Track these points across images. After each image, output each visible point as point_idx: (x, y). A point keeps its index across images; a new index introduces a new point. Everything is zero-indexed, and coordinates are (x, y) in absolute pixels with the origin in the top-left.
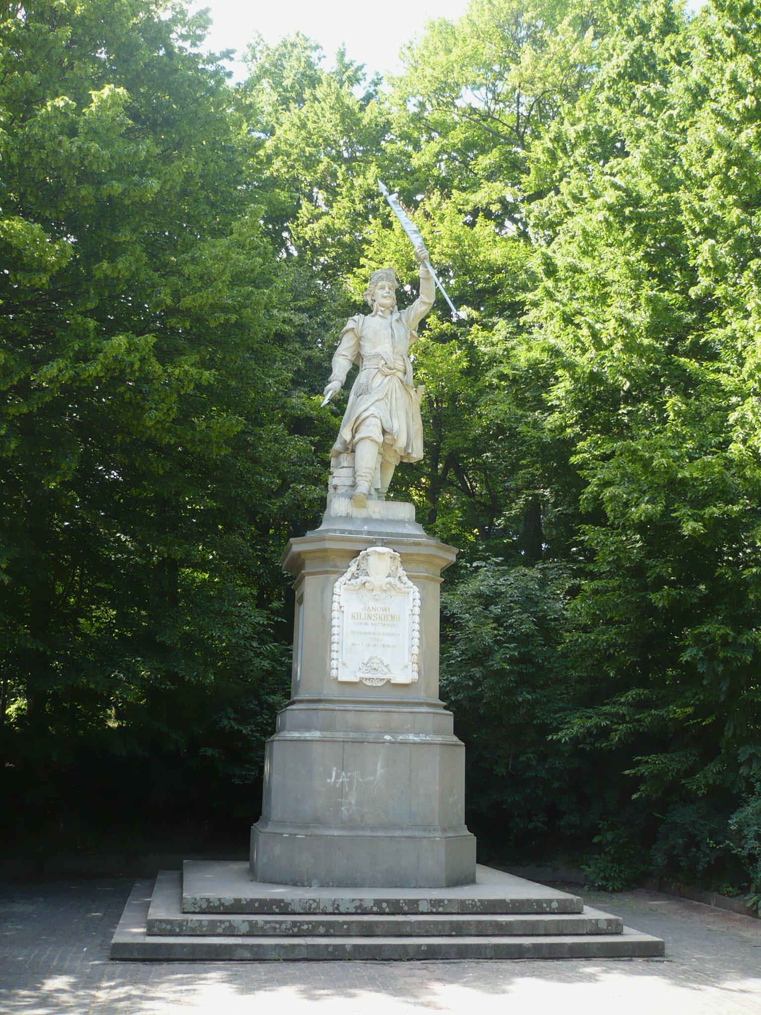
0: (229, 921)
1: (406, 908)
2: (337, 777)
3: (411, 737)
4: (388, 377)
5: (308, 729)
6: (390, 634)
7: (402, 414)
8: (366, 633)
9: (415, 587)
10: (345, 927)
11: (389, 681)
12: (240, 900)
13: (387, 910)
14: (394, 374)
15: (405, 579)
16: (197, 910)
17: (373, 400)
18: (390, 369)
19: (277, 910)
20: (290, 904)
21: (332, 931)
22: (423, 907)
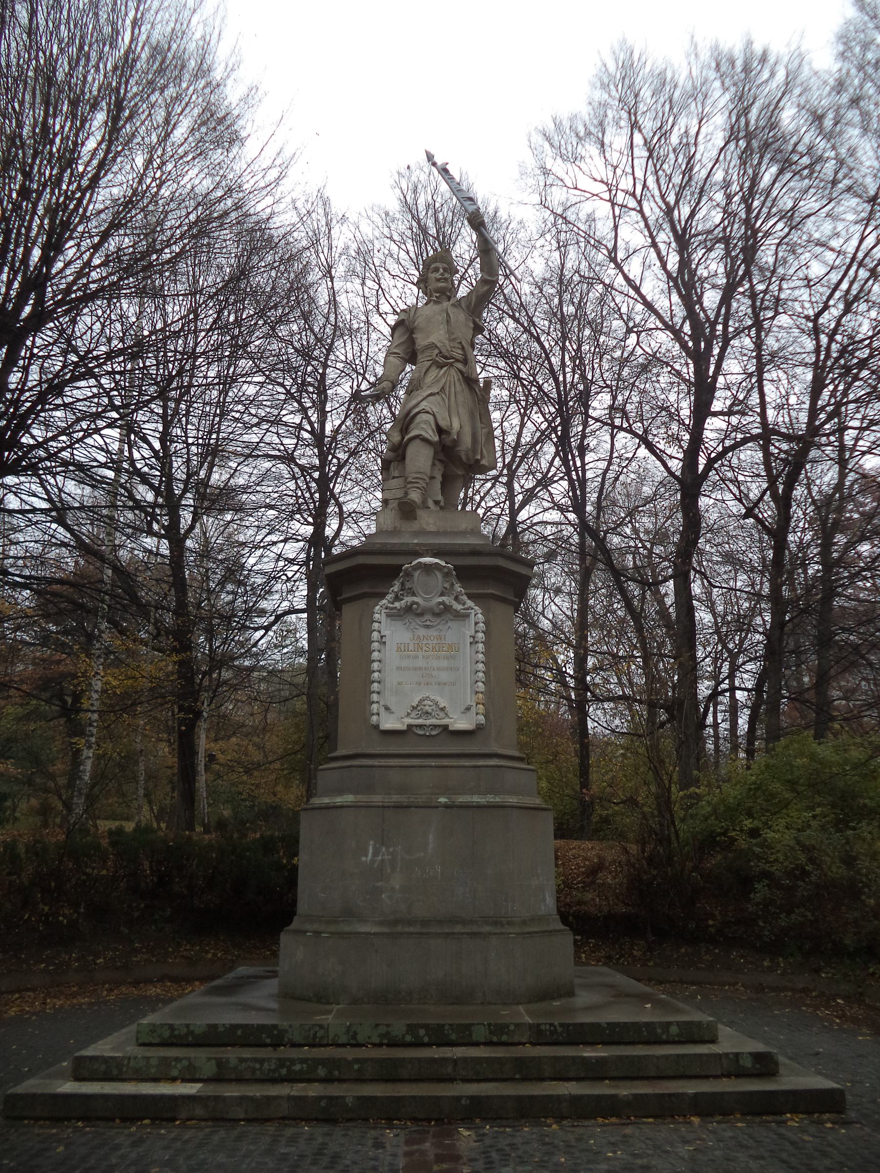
0: (189, 1059)
1: (453, 1037)
2: (376, 853)
3: (476, 799)
5: (341, 792)
6: (446, 669)
8: (415, 669)
10: (356, 1067)
11: (445, 728)
12: (215, 1027)
13: (426, 1040)
14: (451, 365)
15: (465, 598)
16: (157, 1041)
18: (446, 358)
19: (268, 1041)
20: (286, 1031)
21: (336, 1073)
22: (480, 1033)
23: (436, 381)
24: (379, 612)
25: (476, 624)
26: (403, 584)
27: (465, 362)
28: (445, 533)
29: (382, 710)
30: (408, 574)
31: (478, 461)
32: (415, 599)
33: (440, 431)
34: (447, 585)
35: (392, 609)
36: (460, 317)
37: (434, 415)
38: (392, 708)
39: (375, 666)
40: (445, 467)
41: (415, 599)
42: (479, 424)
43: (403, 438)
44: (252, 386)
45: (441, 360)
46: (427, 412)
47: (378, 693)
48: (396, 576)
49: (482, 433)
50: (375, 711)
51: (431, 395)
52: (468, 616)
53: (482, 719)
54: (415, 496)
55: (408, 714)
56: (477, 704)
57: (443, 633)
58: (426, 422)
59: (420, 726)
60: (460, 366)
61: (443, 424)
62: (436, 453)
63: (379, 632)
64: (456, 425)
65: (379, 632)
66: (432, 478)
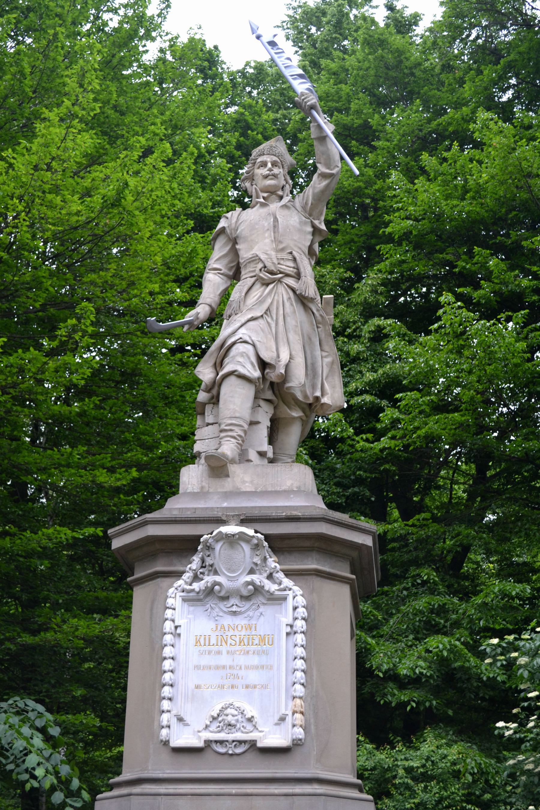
4: (271, 286)
6: (256, 667)
7: (296, 339)
8: (217, 668)
9: (296, 588)
11: (253, 744)
14: (279, 281)
15: (281, 575)
17: (243, 320)
18: (272, 273)
23: (261, 301)
24: (174, 594)
25: (295, 608)
26: (203, 561)
28: (264, 494)
29: (174, 721)
30: (209, 548)
31: (317, 399)
32: (218, 578)
33: (263, 365)
34: (257, 560)
37: (254, 345)
38: (187, 718)
39: (167, 665)
40: (275, 408)
41: (218, 578)
44: (291, 264)
46: (246, 342)
47: (170, 699)
48: (195, 551)
50: (165, 723)
52: (285, 599)
53: (299, 733)
55: (207, 727)
56: (294, 712)
57: (253, 622)
58: (242, 354)
59: (221, 742)
60: (291, 281)
61: (267, 356)
63: (173, 621)
64: (284, 357)
65: (173, 621)
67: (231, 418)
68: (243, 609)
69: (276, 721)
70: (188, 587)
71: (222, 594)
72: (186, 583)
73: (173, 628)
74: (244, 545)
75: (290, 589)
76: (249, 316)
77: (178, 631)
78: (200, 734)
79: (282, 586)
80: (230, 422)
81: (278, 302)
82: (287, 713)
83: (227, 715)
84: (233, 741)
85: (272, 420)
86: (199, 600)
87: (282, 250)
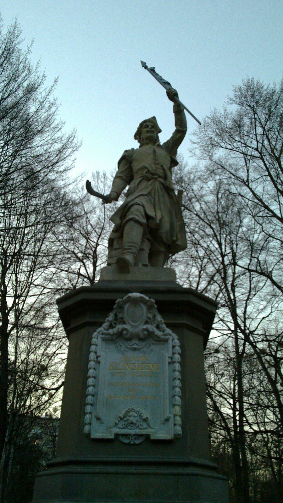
4: (152, 181)
9: (174, 335)
11: (147, 437)
14: (156, 179)
15: (164, 326)
25: (173, 347)
26: (116, 315)
27: (165, 177)
30: (121, 307)
31: (174, 242)
32: (125, 326)
34: (150, 316)
35: (106, 334)
36: (162, 153)
37: (143, 207)
40: (152, 245)
41: (125, 326)
42: (174, 218)
43: (122, 221)
44: (162, 171)
45: (149, 176)
46: (139, 204)
47: (92, 405)
48: (111, 309)
49: (177, 224)
51: (142, 195)
52: (167, 341)
54: (129, 258)
55: (116, 424)
56: (175, 416)
58: (138, 210)
59: (126, 435)
62: (144, 233)
63: (96, 353)
65: (96, 353)
66: (142, 250)
67: (130, 242)
68: (140, 347)
69: (162, 422)
70: (106, 332)
71: (127, 336)
72: (105, 329)
73: (95, 358)
74: (142, 305)
75: (170, 335)
76: (140, 193)
77: (99, 359)
78: (111, 429)
79: (165, 333)
80: (130, 244)
81: (155, 189)
82: (170, 415)
83: (130, 416)
84: (134, 435)
85: (150, 250)
86: (112, 340)
87: (158, 164)
